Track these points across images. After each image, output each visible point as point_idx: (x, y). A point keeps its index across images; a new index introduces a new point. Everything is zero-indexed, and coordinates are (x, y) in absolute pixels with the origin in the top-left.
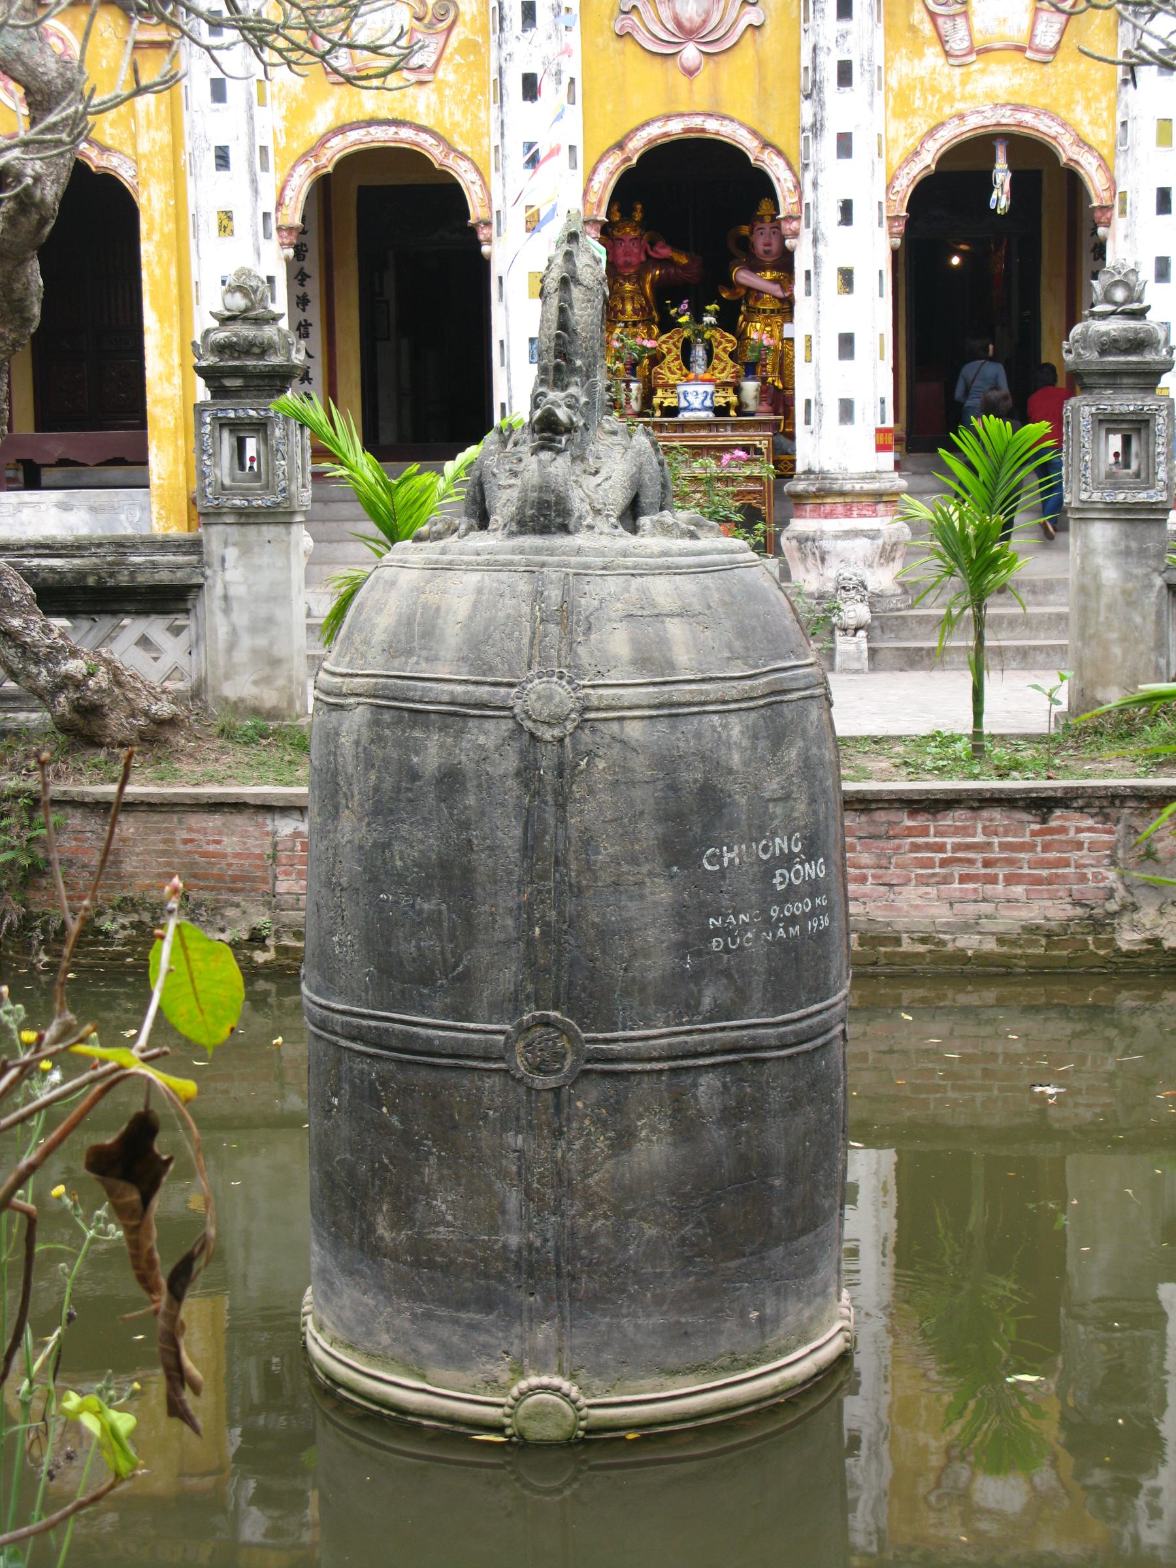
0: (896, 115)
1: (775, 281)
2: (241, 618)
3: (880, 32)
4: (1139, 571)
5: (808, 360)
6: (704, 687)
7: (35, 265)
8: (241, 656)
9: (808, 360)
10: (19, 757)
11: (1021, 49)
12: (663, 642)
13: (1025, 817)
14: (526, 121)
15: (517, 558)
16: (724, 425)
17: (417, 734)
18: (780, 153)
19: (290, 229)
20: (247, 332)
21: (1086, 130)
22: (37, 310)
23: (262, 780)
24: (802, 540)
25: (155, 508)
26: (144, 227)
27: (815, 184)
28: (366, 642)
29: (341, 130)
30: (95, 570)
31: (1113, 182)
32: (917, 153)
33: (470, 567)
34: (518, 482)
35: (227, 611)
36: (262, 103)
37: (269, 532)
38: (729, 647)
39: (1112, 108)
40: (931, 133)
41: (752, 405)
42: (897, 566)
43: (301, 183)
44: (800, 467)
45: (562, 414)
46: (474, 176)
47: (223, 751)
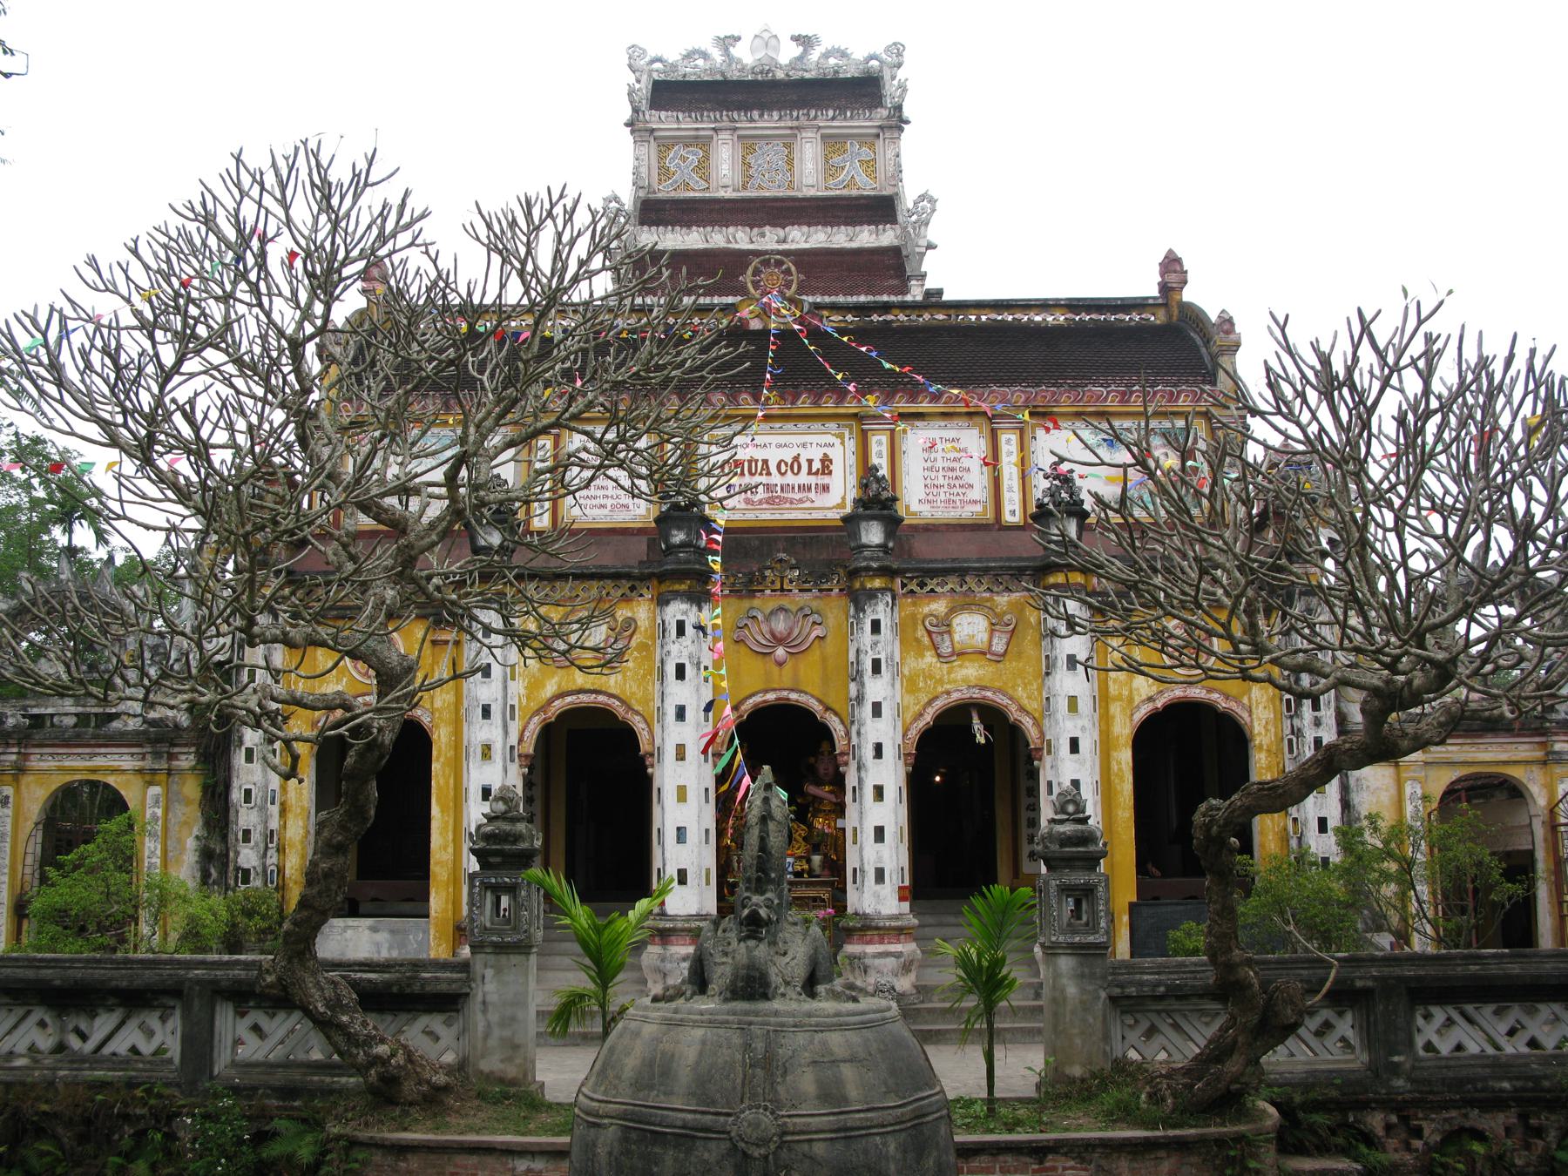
0: (908, 692)
1: (831, 792)
2: (494, 1017)
3: (897, 643)
4: (1090, 988)
5: (855, 843)
6: (870, 1115)
7: (374, 784)
8: (492, 1042)
9: (855, 843)
10: (341, 1109)
11: (984, 653)
12: (839, 1082)
13: (1028, 1160)
14: (678, 692)
15: (731, 1018)
16: (801, 883)
17: (657, 1150)
18: (836, 714)
19: (527, 756)
20: (506, 827)
21: (1025, 702)
22: (372, 812)
23: (506, 1131)
24: (852, 958)
25: (432, 932)
26: (434, 753)
27: (859, 733)
28: (618, 1077)
29: (561, 695)
30: (398, 982)
31: (1042, 734)
32: (921, 715)
33: (696, 1024)
34: (730, 960)
35: (485, 1011)
36: (513, 679)
37: (515, 959)
38: (885, 1083)
39: (1040, 690)
40: (930, 703)
41: (818, 871)
42: (912, 976)
43: (535, 726)
44: (850, 910)
45: (763, 912)
46: (643, 725)
47: (479, 1109)
